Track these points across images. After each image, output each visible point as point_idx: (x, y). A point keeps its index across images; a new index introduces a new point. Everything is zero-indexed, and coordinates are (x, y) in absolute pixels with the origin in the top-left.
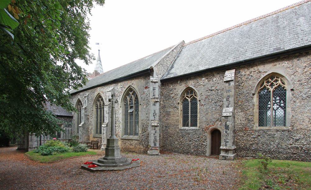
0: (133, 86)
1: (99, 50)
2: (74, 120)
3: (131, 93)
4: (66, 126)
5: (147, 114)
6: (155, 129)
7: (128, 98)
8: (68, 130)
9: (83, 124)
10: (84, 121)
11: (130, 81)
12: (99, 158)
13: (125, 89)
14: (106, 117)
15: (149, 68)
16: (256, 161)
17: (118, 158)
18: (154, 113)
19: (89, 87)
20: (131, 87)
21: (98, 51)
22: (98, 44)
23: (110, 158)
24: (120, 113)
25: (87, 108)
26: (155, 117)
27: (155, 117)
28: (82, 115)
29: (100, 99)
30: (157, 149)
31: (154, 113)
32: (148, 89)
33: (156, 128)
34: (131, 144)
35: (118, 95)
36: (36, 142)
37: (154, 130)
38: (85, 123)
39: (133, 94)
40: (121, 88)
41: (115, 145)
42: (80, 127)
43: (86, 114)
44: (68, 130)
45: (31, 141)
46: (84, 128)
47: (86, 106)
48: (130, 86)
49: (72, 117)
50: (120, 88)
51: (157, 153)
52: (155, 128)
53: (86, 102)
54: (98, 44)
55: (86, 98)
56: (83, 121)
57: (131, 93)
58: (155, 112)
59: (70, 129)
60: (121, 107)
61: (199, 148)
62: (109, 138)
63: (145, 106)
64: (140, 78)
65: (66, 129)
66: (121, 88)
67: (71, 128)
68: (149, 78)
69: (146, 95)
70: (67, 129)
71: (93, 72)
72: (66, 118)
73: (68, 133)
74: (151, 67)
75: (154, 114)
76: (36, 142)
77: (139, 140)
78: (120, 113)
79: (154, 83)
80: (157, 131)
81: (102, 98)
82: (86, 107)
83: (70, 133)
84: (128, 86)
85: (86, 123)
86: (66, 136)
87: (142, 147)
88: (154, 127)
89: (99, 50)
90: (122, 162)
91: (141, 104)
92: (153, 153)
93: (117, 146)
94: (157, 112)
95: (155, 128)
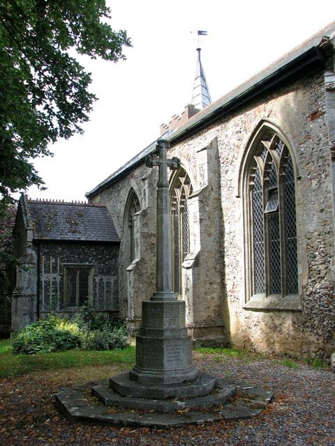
0: (269, 119)
1: (199, 50)
2: (122, 253)
3: (267, 144)
4: (102, 273)
5: (322, 211)
7: (260, 162)
8: (107, 282)
9: (137, 263)
10: (141, 254)
11: (262, 107)
12: (114, 372)
13: (250, 134)
14: (195, 236)
15: (315, 45)
17: (179, 376)
19: (298, 209)
20: (265, 124)
21: (197, 52)
22: (200, 33)
23: (145, 374)
24: (236, 218)
25: (149, 211)
28: (137, 236)
29: (182, 180)
32: (319, 120)
34: (275, 327)
35: (230, 158)
36: (28, 316)
38: (142, 259)
39: (274, 147)
40: (237, 133)
41: (166, 325)
42: (129, 271)
43: (146, 230)
44: (108, 283)
45: (16, 311)
46: (140, 275)
47: (147, 206)
48: (262, 121)
49: (117, 244)
50: (234, 136)
53: (147, 194)
54: (200, 33)
55: (147, 181)
56: (139, 254)
57: (267, 144)
59: (112, 279)
60: (238, 197)
62: (149, 301)
63: (314, 182)
64: (291, 88)
65: (101, 280)
66: (237, 133)
67: (115, 278)
68: (320, 80)
69: (316, 140)
70: (105, 279)
71: (183, 110)
72: (102, 248)
73: (107, 292)
74: (323, 41)
76: (28, 316)
77: (300, 311)
78: (236, 218)
81: (188, 177)
82: (144, 211)
83: (112, 291)
84: (256, 123)
85: (147, 258)
86: (101, 301)
87: (313, 338)
89: (199, 50)
91: (299, 178)
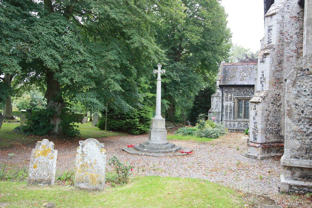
6: (255, 109)
16: (141, 79)
18: (261, 78)
26: (263, 85)
27: (263, 85)
30: (256, 147)
31: (261, 78)
33: (256, 105)
37: (254, 110)
51: (256, 155)
52: (255, 106)
58: (263, 75)
61: (9, 71)
75: (262, 80)
79: (269, 18)
80: (258, 113)
88: (254, 104)
90: (152, 148)
92: (250, 154)
93: (155, 128)
94: (267, 74)
95: (255, 106)
